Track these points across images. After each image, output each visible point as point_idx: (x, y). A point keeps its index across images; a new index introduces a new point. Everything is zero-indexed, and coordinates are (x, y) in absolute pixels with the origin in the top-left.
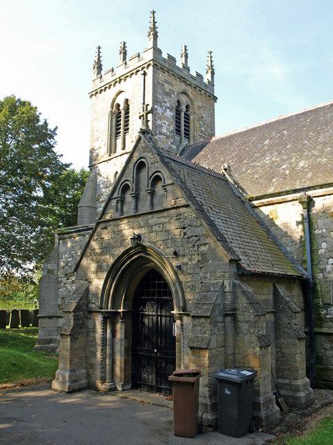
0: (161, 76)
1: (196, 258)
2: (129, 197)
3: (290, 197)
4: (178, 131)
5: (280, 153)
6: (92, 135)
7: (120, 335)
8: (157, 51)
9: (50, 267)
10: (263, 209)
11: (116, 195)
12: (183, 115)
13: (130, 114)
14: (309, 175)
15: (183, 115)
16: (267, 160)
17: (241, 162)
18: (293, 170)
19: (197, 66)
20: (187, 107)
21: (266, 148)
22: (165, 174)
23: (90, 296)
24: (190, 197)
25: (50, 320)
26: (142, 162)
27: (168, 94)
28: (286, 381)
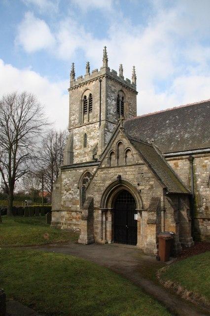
0: (110, 83)
1: (148, 187)
2: (113, 157)
3: (184, 157)
4: (118, 111)
5: (175, 128)
6: (70, 113)
7: (110, 219)
8: (108, 69)
9: (96, 188)
10: (169, 162)
11: (107, 156)
12: (120, 102)
13: (93, 102)
14: (190, 142)
15: (120, 102)
16: (168, 132)
17: (154, 132)
18: (182, 137)
19: (127, 75)
20: (123, 98)
21: (167, 125)
22: (132, 148)
23: (94, 202)
24: (145, 160)
25: (57, 213)
26: (120, 143)
27: (113, 92)
28: (183, 238)
